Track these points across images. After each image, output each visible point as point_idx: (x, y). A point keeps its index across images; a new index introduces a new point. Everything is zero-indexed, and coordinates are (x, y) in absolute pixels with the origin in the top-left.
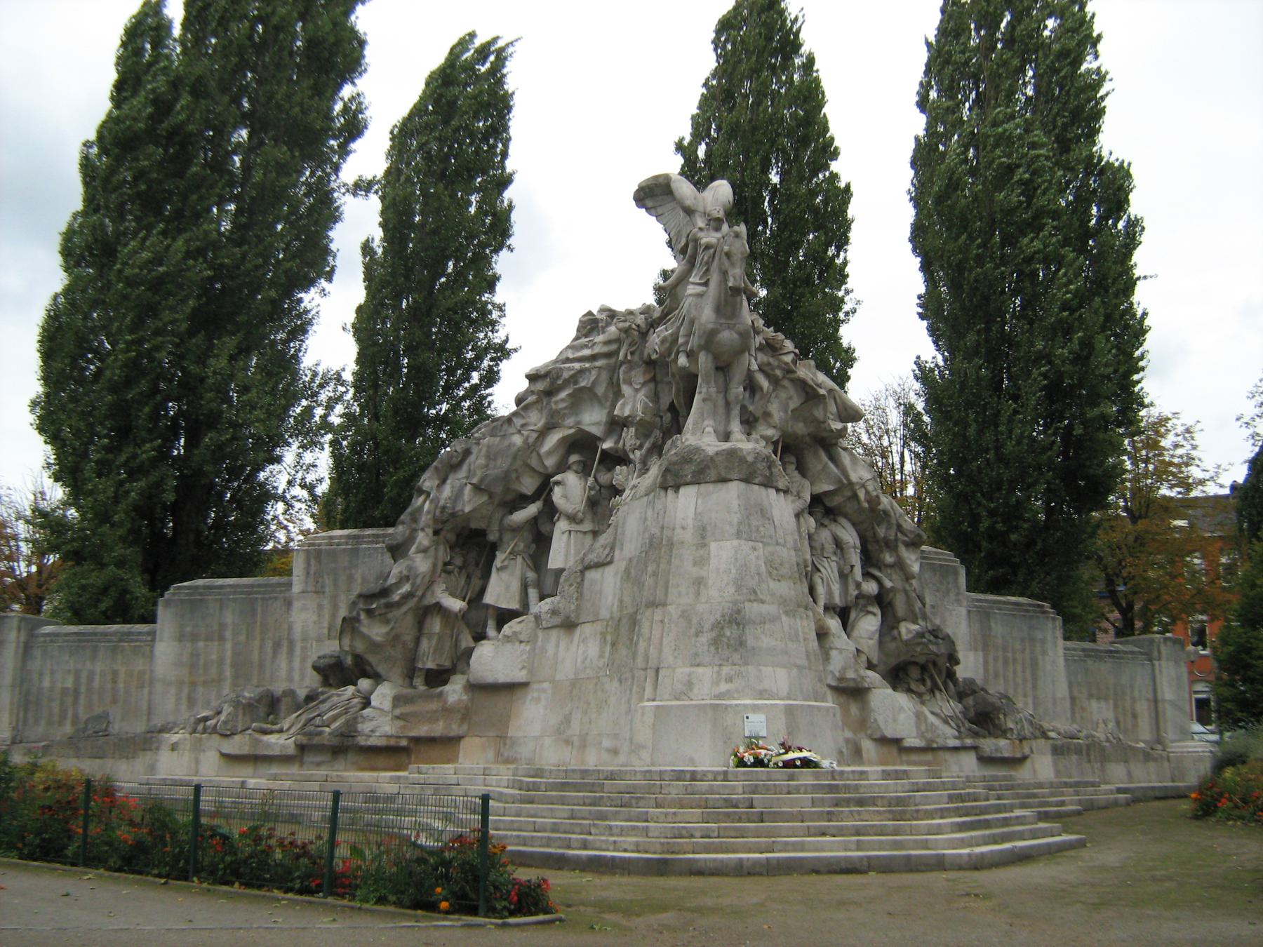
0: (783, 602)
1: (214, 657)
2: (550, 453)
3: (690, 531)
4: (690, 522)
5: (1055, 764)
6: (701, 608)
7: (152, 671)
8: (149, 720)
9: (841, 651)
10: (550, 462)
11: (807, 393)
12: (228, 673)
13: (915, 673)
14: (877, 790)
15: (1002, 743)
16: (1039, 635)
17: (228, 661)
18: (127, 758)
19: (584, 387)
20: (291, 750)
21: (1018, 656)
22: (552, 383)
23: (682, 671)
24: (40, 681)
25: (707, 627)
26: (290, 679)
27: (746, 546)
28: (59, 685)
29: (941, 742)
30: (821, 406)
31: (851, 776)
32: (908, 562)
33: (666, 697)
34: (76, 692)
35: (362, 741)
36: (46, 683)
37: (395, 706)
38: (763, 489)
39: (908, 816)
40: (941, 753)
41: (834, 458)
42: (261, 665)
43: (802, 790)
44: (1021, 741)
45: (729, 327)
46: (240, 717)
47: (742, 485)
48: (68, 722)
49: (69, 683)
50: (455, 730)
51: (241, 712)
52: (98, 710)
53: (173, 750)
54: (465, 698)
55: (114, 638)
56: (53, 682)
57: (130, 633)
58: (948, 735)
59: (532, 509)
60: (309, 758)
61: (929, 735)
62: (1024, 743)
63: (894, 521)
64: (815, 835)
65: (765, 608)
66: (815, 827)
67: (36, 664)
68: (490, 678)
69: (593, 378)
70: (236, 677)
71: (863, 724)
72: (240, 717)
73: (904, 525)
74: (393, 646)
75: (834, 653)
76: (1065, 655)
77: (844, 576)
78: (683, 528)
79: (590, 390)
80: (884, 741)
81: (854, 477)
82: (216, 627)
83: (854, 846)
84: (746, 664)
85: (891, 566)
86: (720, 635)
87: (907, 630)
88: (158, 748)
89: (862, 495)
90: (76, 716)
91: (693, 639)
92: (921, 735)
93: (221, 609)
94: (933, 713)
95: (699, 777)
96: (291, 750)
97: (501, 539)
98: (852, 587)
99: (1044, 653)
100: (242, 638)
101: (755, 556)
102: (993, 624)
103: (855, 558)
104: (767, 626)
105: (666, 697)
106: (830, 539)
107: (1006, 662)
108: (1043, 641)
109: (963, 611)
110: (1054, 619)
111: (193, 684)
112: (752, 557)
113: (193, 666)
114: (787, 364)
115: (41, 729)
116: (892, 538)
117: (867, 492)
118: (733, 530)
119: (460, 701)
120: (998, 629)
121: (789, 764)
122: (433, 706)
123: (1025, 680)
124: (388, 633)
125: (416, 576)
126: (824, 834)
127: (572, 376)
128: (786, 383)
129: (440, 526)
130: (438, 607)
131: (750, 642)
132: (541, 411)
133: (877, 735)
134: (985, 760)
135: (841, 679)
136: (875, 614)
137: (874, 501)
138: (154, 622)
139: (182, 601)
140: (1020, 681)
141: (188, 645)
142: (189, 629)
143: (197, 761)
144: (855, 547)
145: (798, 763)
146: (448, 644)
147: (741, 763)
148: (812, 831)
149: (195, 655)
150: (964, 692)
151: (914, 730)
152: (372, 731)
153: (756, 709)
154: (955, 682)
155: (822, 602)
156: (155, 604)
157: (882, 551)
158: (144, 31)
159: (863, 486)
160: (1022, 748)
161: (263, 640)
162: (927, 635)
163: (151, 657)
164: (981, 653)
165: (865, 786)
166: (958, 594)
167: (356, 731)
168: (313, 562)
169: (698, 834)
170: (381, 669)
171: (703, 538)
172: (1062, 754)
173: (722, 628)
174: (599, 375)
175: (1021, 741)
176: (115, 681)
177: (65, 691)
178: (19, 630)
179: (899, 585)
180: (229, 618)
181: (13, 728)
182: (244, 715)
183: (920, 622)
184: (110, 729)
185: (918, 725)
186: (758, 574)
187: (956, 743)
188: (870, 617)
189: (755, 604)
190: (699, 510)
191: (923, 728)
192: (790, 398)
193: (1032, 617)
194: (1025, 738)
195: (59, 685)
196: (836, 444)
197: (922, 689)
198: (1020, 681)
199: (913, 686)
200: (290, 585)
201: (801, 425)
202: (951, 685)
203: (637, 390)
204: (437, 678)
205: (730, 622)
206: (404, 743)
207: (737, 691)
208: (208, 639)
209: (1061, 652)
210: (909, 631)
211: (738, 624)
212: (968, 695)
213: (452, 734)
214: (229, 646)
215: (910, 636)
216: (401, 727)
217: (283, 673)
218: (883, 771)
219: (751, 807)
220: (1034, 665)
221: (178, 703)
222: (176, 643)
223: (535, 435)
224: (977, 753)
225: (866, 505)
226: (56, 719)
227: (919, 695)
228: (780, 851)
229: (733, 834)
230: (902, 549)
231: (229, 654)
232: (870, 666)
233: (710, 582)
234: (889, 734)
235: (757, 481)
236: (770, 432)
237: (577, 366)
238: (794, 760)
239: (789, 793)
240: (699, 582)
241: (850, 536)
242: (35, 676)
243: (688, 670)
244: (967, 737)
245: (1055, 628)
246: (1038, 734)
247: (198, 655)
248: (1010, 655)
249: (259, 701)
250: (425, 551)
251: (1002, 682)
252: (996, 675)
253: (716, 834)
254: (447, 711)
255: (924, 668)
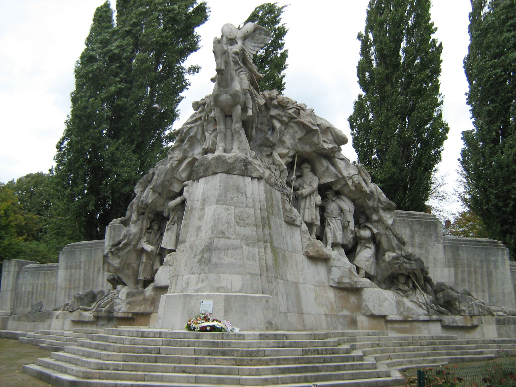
0: (246, 239)
1: (77, 276)
2: (183, 171)
3: (200, 201)
4: (200, 197)
5: (498, 330)
6: (198, 242)
7: (57, 283)
8: (55, 305)
9: (339, 268)
10: (184, 175)
11: (306, 129)
12: (82, 284)
13: (402, 279)
14: (242, 346)
15: (458, 318)
16: (493, 258)
17: (82, 278)
18: (43, 322)
19: (192, 136)
20: (92, 319)
21: (478, 270)
22: (181, 136)
23: (186, 276)
24: (22, 288)
25: (198, 252)
26: (103, 286)
27: (221, 208)
28: (27, 290)
29: (414, 317)
30: (316, 136)
31: (233, 337)
32: (385, 218)
33: (178, 291)
34: (33, 293)
35: (115, 314)
36: (23, 289)
37: (127, 298)
38: (241, 177)
39: (245, 363)
40: (416, 324)
41: (334, 165)
42: (93, 280)
43: (197, 344)
44: (471, 317)
45: (226, 93)
46: (76, 304)
47: (224, 176)
48: (30, 306)
49: (30, 290)
50: (148, 309)
51: (76, 301)
52: (39, 301)
53: (57, 318)
54: (153, 293)
55: (46, 269)
56: (25, 289)
57: (51, 267)
58: (421, 313)
59: (178, 200)
60: (100, 322)
61: (405, 314)
62: (474, 318)
63: (376, 197)
64: (179, 372)
65: (229, 242)
66: (179, 367)
67: (20, 281)
68: (160, 285)
69: (195, 131)
70: (84, 285)
71: (359, 307)
72: (76, 304)
73: (381, 199)
74: (128, 269)
75: (334, 269)
76: (511, 269)
77: (345, 228)
78: (197, 201)
79: (195, 137)
80: (373, 316)
81: (345, 173)
82: (78, 263)
83: (193, 380)
84: (210, 272)
85: (375, 221)
86: (203, 257)
87: (389, 256)
88: (52, 318)
89: (350, 183)
90: (32, 303)
91: (192, 260)
92: (401, 314)
93: (80, 254)
94: (412, 301)
95: (145, 335)
96: (92, 319)
97: (169, 214)
98: (349, 233)
99: (496, 268)
100: (87, 267)
101: (228, 214)
102: (460, 253)
103: (351, 218)
104: (229, 252)
105: (178, 291)
106: (336, 207)
107: (470, 273)
108: (496, 262)
109: (441, 246)
110: (503, 249)
111: (70, 288)
112: (225, 214)
113: (70, 281)
114: (290, 114)
115: (21, 309)
116: (375, 206)
117: (353, 182)
118: (214, 199)
119: (151, 295)
120: (464, 255)
121: (203, 329)
122: (141, 298)
123: (483, 283)
124: (120, 263)
125: (130, 235)
126: (184, 372)
127: (187, 131)
128: (292, 124)
129: (143, 211)
130: (143, 250)
131: (214, 260)
132: (180, 150)
133: (369, 314)
134: (446, 327)
135: (339, 283)
136: (370, 248)
137: (358, 187)
138: (58, 262)
139: (68, 251)
140: (479, 283)
141: (69, 271)
142: (69, 264)
143: (64, 323)
144: (350, 212)
145: (208, 328)
146: (149, 267)
147: (189, 328)
148: (177, 369)
149: (71, 276)
150: (438, 290)
151: (396, 310)
152: (119, 310)
153: (208, 297)
154: (432, 285)
155: (330, 242)
156: (58, 254)
157: (373, 214)
158: (102, 16)
159: (351, 178)
160: (472, 321)
161: (94, 268)
162: (401, 259)
163: (56, 277)
164: (452, 270)
165: (235, 343)
166: (437, 237)
167: (113, 310)
168: (112, 231)
169: (111, 368)
170: (124, 280)
171: (204, 205)
172: (504, 324)
173: (204, 253)
174: (197, 129)
175: (471, 317)
176: (45, 288)
177: (29, 291)
178: (15, 266)
179: (382, 231)
180: (83, 258)
181: (11, 309)
182: (78, 302)
183: (397, 251)
184: (42, 309)
185: (398, 308)
186: (228, 223)
187: (427, 318)
188: (368, 249)
189: (222, 239)
190: (205, 190)
191: (402, 309)
192: (296, 132)
193: (487, 249)
194: (474, 315)
195: (27, 290)
196: (334, 157)
197: (406, 288)
198: (479, 283)
199: (401, 287)
200: (104, 243)
201: (308, 147)
202: (429, 286)
203: (211, 134)
204: (146, 283)
205: (207, 250)
206: (130, 315)
207: (204, 288)
208: (76, 268)
209: (508, 267)
210: (389, 257)
211: (210, 251)
212: (440, 292)
213: (147, 311)
214: (82, 271)
215: (390, 259)
216: (129, 308)
217: (100, 283)
218: (260, 335)
219: (159, 353)
220: (490, 274)
221: (65, 298)
222: (64, 271)
223: (176, 162)
224: (441, 324)
225: (353, 188)
226: (26, 304)
227: (405, 292)
228: (148, 381)
229: (130, 369)
230: (381, 212)
231: (82, 275)
232: (368, 276)
233: (203, 228)
234: (376, 312)
235: (236, 173)
236: (285, 151)
237: (189, 126)
238: (206, 327)
239: (189, 346)
240: (199, 228)
241: (348, 206)
242: (20, 286)
243: (188, 276)
244: (433, 314)
245: (504, 254)
246: (486, 313)
247: (72, 275)
248: (472, 269)
249: (86, 295)
250: (135, 222)
251: (467, 283)
252: (463, 281)
253: (121, 368)
254: (145, 300)
255: (408, 277)
